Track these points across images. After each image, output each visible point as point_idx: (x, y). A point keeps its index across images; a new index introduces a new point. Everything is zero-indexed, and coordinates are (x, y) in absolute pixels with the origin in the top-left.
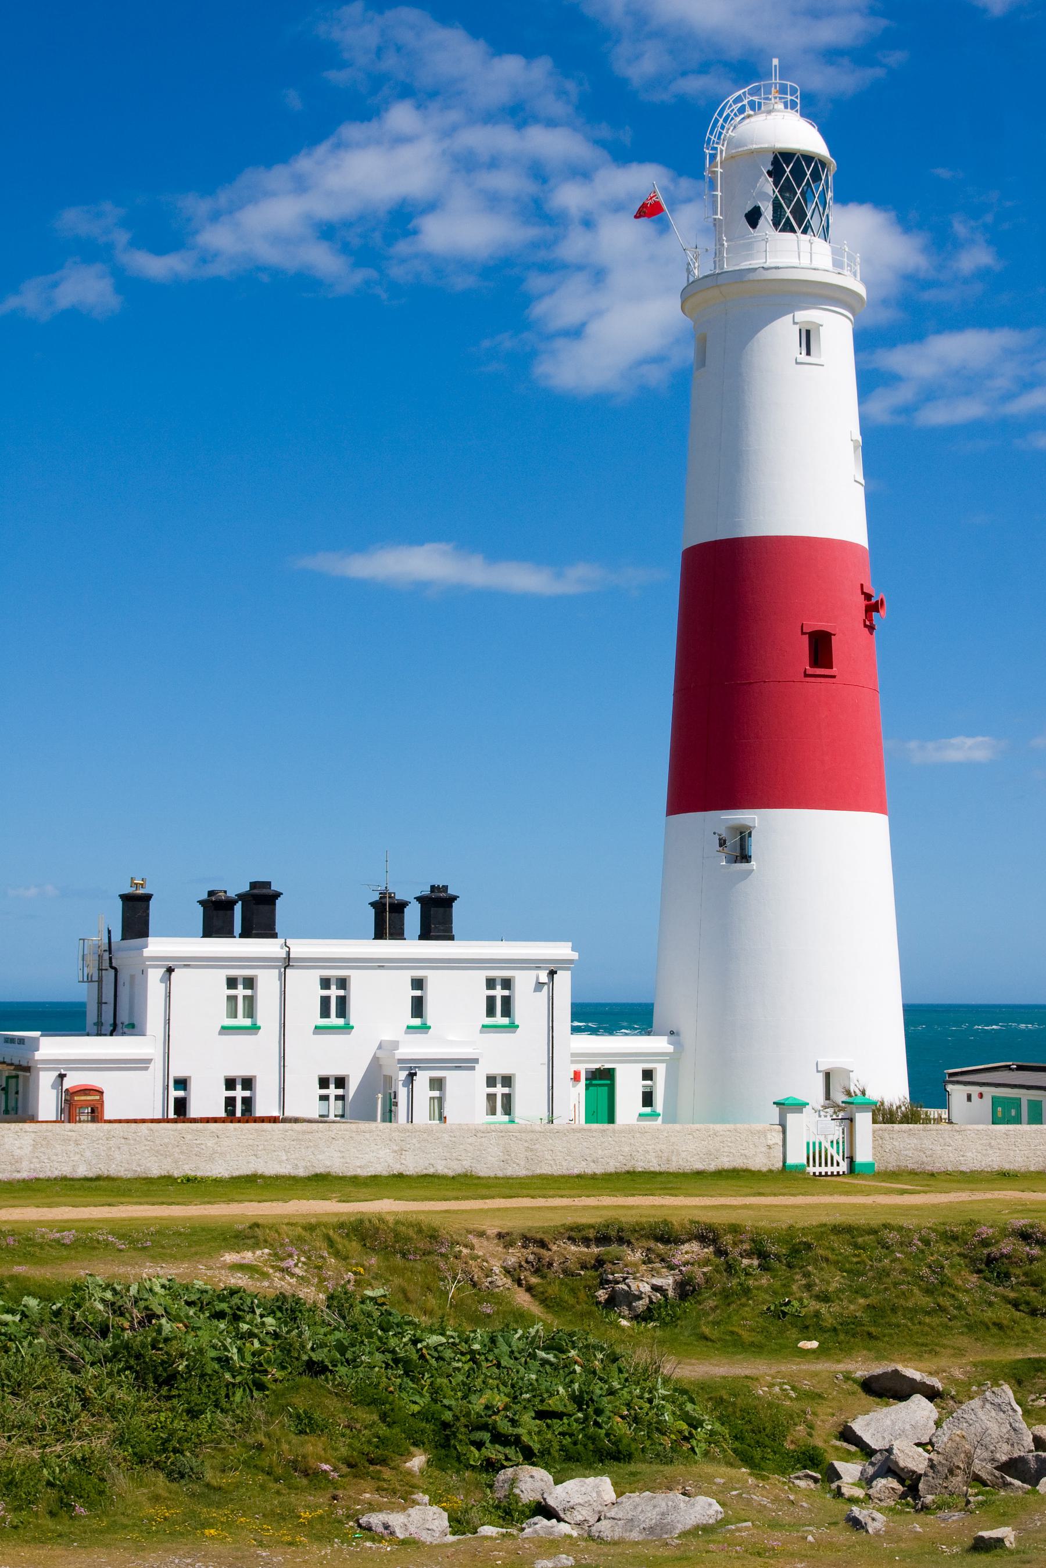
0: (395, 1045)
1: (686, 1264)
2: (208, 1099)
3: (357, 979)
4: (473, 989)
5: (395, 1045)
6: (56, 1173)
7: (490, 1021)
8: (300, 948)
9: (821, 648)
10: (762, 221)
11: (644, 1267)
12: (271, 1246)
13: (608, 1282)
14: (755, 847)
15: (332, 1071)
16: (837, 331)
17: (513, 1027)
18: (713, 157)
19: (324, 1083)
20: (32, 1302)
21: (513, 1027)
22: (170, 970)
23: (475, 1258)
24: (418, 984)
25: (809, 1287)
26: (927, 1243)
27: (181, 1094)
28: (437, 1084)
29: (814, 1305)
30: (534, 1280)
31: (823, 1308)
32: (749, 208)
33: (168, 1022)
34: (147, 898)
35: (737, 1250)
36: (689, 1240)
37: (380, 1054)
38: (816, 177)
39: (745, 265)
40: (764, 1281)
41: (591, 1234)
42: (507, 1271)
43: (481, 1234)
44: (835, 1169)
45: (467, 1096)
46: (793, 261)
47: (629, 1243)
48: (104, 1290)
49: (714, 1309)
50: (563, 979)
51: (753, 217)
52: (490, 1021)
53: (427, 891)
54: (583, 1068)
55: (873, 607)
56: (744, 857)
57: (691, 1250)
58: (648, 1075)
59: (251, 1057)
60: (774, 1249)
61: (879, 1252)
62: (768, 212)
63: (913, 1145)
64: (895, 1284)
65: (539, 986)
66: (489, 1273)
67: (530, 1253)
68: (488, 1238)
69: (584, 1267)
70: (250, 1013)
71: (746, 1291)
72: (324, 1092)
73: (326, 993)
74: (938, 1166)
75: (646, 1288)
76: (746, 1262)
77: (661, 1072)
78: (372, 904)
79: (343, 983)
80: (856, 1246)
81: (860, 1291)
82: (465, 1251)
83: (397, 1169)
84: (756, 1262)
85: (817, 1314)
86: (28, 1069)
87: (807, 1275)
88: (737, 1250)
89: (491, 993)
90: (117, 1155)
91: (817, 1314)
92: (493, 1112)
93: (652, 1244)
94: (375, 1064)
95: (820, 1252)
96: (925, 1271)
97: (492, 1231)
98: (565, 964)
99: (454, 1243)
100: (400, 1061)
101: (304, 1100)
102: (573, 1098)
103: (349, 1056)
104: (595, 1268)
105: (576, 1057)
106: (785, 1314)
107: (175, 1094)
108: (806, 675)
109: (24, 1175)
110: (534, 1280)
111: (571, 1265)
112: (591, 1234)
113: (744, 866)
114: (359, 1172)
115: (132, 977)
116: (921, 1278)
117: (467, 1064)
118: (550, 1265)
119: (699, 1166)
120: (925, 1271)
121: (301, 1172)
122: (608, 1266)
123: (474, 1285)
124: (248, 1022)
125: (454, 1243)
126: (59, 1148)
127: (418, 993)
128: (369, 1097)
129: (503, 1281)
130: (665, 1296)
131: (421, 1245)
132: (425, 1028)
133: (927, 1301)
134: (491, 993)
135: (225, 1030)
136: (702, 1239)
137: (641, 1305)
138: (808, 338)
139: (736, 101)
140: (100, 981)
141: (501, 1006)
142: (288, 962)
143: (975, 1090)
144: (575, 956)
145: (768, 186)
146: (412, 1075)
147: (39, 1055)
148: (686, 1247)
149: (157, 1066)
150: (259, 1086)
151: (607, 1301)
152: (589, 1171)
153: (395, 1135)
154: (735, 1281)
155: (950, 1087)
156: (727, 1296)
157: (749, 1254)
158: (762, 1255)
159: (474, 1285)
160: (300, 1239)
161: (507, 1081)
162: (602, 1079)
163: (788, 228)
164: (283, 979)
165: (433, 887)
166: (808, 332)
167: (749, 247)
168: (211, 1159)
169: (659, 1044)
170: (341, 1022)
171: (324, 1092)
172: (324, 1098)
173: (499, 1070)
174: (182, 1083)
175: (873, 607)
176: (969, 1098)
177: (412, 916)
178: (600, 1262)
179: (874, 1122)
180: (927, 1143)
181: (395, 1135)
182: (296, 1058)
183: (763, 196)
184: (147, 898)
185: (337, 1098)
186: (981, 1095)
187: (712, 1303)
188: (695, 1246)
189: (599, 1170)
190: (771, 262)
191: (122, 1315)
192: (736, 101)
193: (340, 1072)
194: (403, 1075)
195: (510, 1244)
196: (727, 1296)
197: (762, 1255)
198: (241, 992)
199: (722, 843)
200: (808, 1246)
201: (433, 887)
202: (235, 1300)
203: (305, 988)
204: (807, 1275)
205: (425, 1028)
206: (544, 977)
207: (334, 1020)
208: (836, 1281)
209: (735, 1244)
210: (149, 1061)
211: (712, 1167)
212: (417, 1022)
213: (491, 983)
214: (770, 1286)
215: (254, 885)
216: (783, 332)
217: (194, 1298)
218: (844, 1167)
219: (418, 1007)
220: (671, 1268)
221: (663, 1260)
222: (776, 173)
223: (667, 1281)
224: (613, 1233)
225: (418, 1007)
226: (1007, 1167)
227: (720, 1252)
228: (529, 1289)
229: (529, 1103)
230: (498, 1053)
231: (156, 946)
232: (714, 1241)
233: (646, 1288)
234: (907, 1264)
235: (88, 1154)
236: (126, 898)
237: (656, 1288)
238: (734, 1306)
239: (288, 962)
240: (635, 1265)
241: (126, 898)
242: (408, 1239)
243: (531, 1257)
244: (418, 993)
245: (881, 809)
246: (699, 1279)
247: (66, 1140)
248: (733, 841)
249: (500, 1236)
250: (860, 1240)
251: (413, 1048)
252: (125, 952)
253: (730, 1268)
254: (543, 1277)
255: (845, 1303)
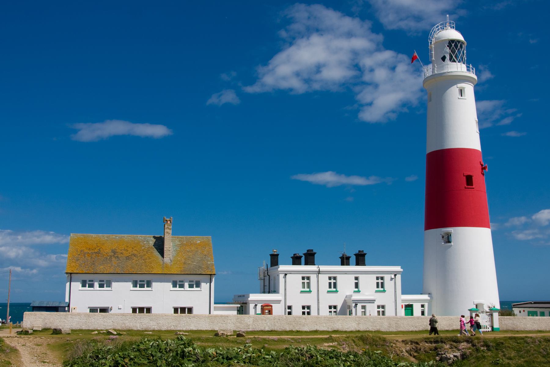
0: (351, 296)
1: (463, 349)
2: (297, 311)
3: (339, 277)
4: (372, 280)
5: (351, 296)
6: (260, 329)
7: (377, 289)
8: (323, 268)
9: (469, 180)
10: (446, 60)
11: (450, 350)
12: (337, 342)
13: (439, 354)
14: (453, 238)
15: (333, 304)
16: (469, 89)
17: (384, 291)
18: (431, 43)
19: (330, 307)
20: (274, 353)
21: (384, 291)
22: (286, 275)
23: (397, 347)
24: (356, 278)
25: (504, 355)
26: (540, 342)
27: (289, 310)
28: (364, 307)
29: (507, 361)
30: (415, 354)
31: (510, 362)
32: (442, 56)
33: (285, 289)
34: (277, 255)
35: (479, 345)
36: (463, 342)
37: (346, 299)
38: (461, 47)
39: (442, 72)
40: (489, 354)
41: (432, 340)
42: (407, 351)
43: (397, 341)
44: (488, 330)
45: (372, 310)
46: (456, 70)
47: (445, 343)
48: (295, 349)
49: (474, 363)
50: (399, 277)
51: (444, 59)
52: (377, 289)
53: (357, 252)
54: (404, 304)
55: (484, 168)
56: (449, 242)
57: (463, 345)
58: (423, 306)
59: (309, 299)
60: (491, 344)
61: (525, 345)
62: (448, 57)
63: (509, 322)
64: (533, 354)
65: (392, 279)
66: (402, 352)
67: (413, 346)
68: (399, 342)
69: (431, 350)
70: (309, 287)
71: (484, 357)
72: (330, 310)
73: (330, 281)
74: (519, 329)
75: (452, 356)
76: (482, 348)
77: (426, 305)
78: (340, 258)
79: (335, 278)
80: (518, 343)
81: (521, 357)
82: (394, 345)
83: (358, 329)
84: (485, 348)
85: (509, 363)
86: (246, 303)
87: (503, 352)
88: (479, 345)
89: (378, 281)
90: (277, 324)
91: (509, 363)
92: (379, 315)
93: (452, 343)
94: (345, 302)
95: (507, 345)
96: (542, 350)
97: (400, 340)
98: (398, 272)
99: (391, 342)
100: (353, 300)
101: (325, 311)
102: (402, 312)
103: (338, 300)
104: (434, 350)
105: (403, 301)
106: (498, 363)
107: (288, 310)
108: (466, 188)
109: (251, 330)
110: (415, 354)
111: (427, 349)
112: (432, 340)
113: (449, 244)
114: (347, 330)
115: (275, 278)
116: (541, 352)
117: (372, 301)
118: (420, 349)
119: (447, 329)
120: (542, 350)
121: (330, 330)
122: (439, 349)
123: (398, 355)
124: (308, 290)
125: (391, 342)
126: (260, 322)
127: (356, 281)
128: (346, 309)
129: (406, 354)
130: (458, 359)
131: (381, 343)
132: (359, 291)
133: (543, 359)
134: (378, 281)
135: (376, 291)
136: (467, 341)
137: (451, 361)
138: (461, 92)
139: (437, 27)
140: (264, 279)
141: (381, 285)
142: (319, 272)
143: (522, 309)
144: (402, 270)
145: (448, 50)
146: (356, 305)
147: (249, 299)
148: (462, 344)
149: (283, 303)
150: (312, 308)
151: (439, 360)
152: (414, 330)
153: (357, 319)
154: (480, 354)
155: (514, 309)
156: (478, 358)
157: (483, 346)
158: (488, 346)
159: (398, 355)
160: (345, 340)
161: (383, 307)
162: (409, 308)
163: (454, 61)
164: (318, 277)
165: (359, 251)
166: (461, 90)
167: (443, 66)
168: (304, 326)
169: (426, 297)
170: (335, 290)
171: (330, 310)
172: (330, 312)
173: (381, 304)
174: (290, 307)
175: (484, 168)
176: (520, 312)
177: (353, 259)
178: (436, 349)
179: (499, 315)
180: (515, 322)
181: (357, 319)
182: (322, 300)
183: (447, 53)
184: (277, 255)
185: (334, 312)
186: (524, 311)
187: (473, 361)
188: (465, 344)
189: (417, 330)
190: (449, 71)
191: (303, 356)
192: (437, 27)
193: (335, 304)
194: (354, 305)
195: (407, 343)
196: (478, 358)
197: (488, 346)
198: (306, 281)
199: (443, 237)
200: (502, 343)
201: (359, 251)
202: (335, 353)
203: (324, 280)
204: (503, 352)
205: (359, 291)
206: (393, 276)
207: (333, 289)
208: (513, 354)
209: (478, 343)
210: (280, 301)
211: (451, 329)
212: (357, 290)
213: (377, 278)
214: (491, 355)
215: (308, 251)
216: (454, 90)
217: (322, 352)
218: (490, 329)
219: (357, 285)
220: (459, 350)
221: (456, 348)
222: (450, 46)
223: (458, 354)
224: (439, 340)
225: (357, 285)
226: (540, 329)
227: (473, 345)
228: (414, 357)
229: (390, 312)
230: (380, 299)
231: (282, 268)
232: (471, 342)
233: (452, 356)
234: (536, 348)
235: (269, 324)
236: (272, 255)
237: (455, 356)
238: (480, 362)
239: (319, 272)
240: (447, 349)
241: (272, 255)
242: (377, 341)
243: (414, 347)
244: (356, 281)
245: (489, 227)
246: (468, 353)
247: (262, 320)
248: (446, 237)
249: (403, 341)
250: (518, 341)
251: (356, 297)
252: (272, 270)
253: (477, 350)
254: (418, 353)
255: (517, 360)
